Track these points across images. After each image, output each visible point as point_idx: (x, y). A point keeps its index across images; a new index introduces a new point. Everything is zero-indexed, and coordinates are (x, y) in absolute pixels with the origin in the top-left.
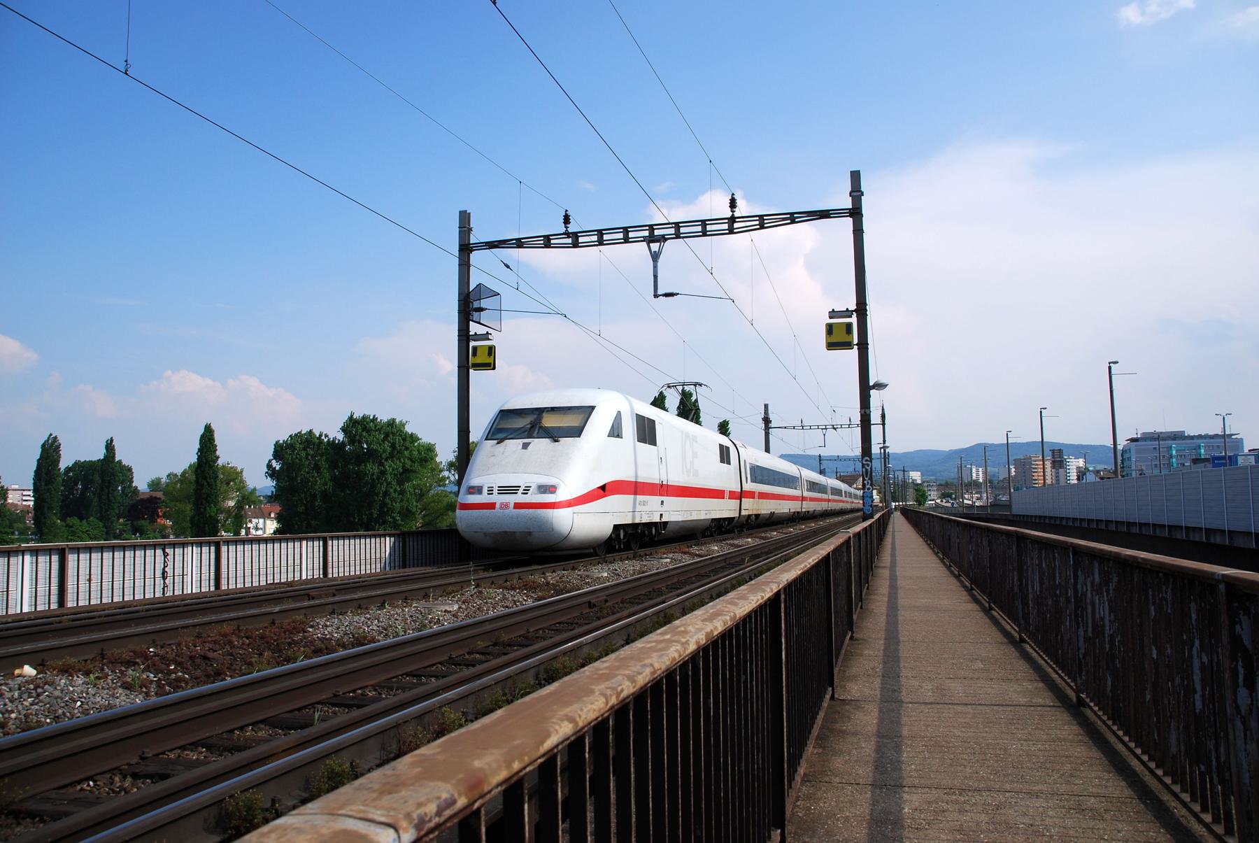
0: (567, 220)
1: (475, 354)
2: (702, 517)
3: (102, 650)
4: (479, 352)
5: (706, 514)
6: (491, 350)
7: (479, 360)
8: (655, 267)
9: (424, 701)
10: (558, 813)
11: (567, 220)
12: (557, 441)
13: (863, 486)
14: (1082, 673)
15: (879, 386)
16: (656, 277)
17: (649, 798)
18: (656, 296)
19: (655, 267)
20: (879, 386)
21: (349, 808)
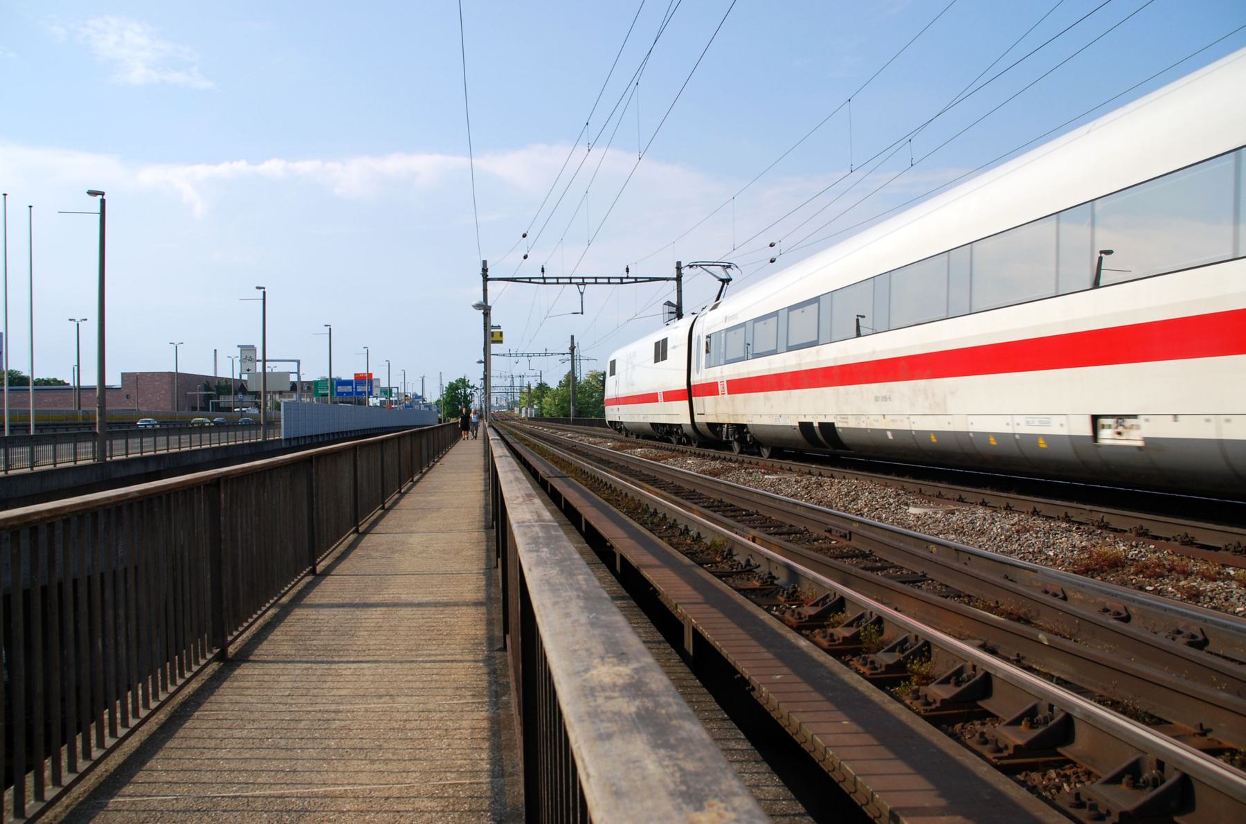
0: (627, 270)
1: (493, 336)
2: (642, 420)
3: (1103, 517)
4: (495, 335)
5: (644, 418)
6: (501, 334)
7: (494, 339)
8: (582, 298)
9: (706, 524)
10: (946, 714)
11: (627, 270)
12: (590, 371)
13: (360, 392)
14: (1033, 668)
15: (480, 362)
16: (582, 302)
17: (941, 715)
18: (582, 313)
19: (582, 298)
20: (480, 362)
21: (141, 420)
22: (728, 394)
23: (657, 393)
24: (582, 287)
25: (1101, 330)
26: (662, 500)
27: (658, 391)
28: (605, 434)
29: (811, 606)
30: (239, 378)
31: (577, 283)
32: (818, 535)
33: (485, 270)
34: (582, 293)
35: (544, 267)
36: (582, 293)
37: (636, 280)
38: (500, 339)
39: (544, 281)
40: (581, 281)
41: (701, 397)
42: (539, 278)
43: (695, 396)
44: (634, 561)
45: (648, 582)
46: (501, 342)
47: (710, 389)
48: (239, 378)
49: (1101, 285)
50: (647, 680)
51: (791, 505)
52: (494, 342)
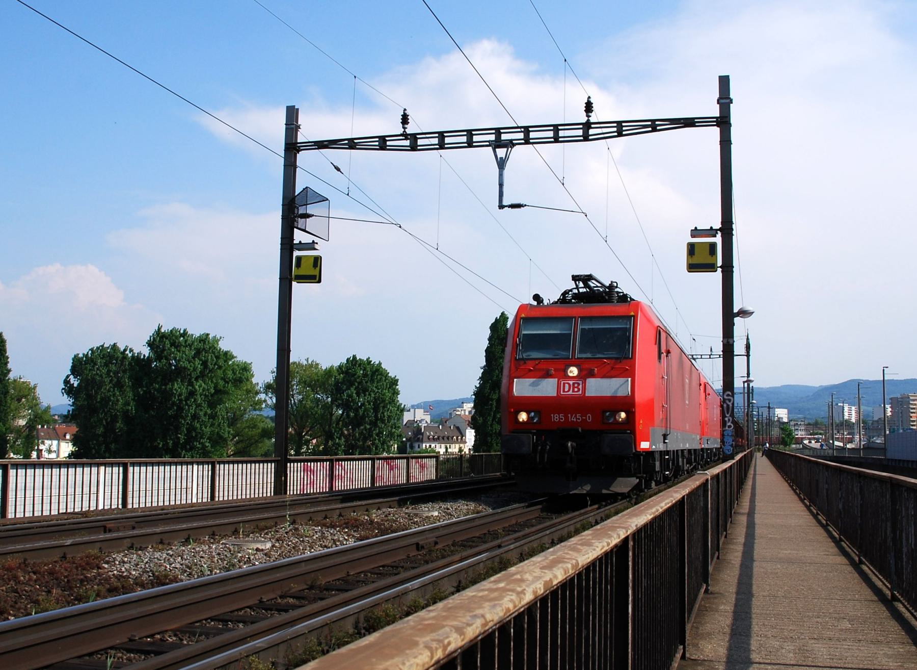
6: (317, 261)
7: (302, 272)
8: (501, 175)
18: (501, 207)
19: (501, 175)
24: (501, 152)
29: (536, 603)
30: (437, 139)
32: (239, 538)
33: (292, 126)
35: (408, 112)
37: (620, 129)
38: (314, 272)
39: (413, 142)
41: (735, 379)
44: (700, 544)
48: (437, 139)
50: (319, 583)
51: (441, 529)
52: (302, 279)
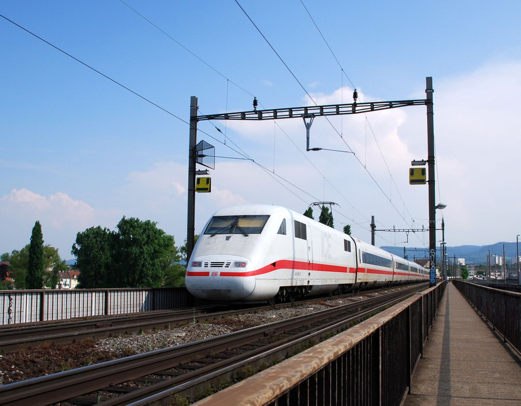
4: (201, 182)
5: (336, 281)
6: (208, 180)
7: (201, 186)
18: (407, 242)
22: (367, 273)
23: (365, 269)
25: (228, 273)
26: (333, 325)
27: (348, 267)
28: (153, 314)
31: (406, 232)
34: (407, 235)
36: (407, 235)
40: (407, 231)
42: (441, 251)
43: (358, 272)
45: (414, 302)
46: (208, 190)
47: (362, 270)
49: (305, 119)
